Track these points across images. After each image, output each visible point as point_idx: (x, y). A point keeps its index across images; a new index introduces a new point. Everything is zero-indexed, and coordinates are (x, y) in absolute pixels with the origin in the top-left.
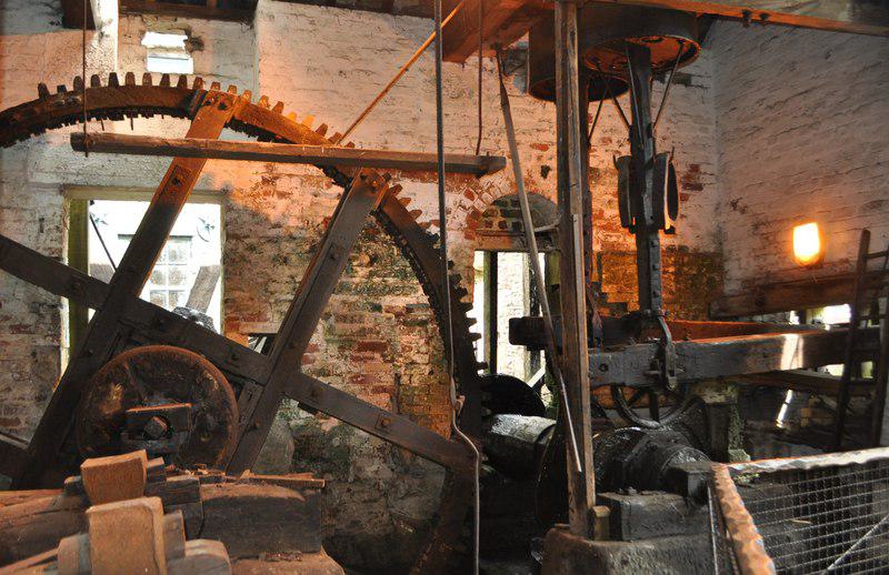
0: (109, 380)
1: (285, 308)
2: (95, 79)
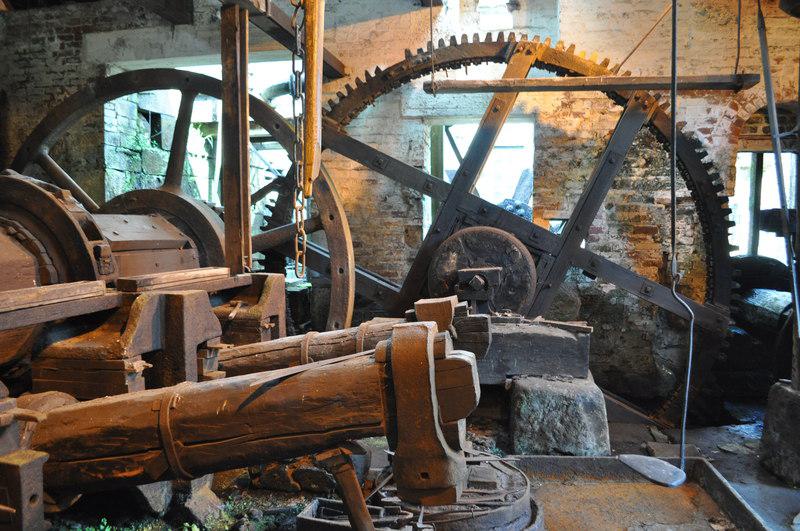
0: (449, 250)
1: (577, 200)
2: (441, 42)
